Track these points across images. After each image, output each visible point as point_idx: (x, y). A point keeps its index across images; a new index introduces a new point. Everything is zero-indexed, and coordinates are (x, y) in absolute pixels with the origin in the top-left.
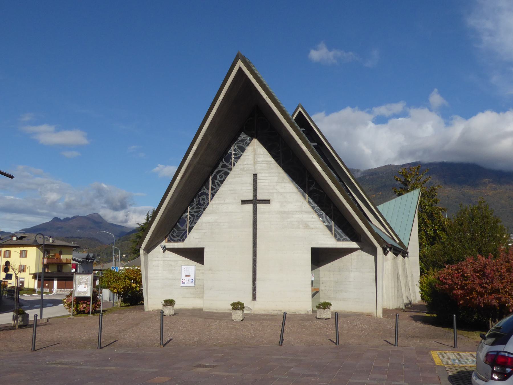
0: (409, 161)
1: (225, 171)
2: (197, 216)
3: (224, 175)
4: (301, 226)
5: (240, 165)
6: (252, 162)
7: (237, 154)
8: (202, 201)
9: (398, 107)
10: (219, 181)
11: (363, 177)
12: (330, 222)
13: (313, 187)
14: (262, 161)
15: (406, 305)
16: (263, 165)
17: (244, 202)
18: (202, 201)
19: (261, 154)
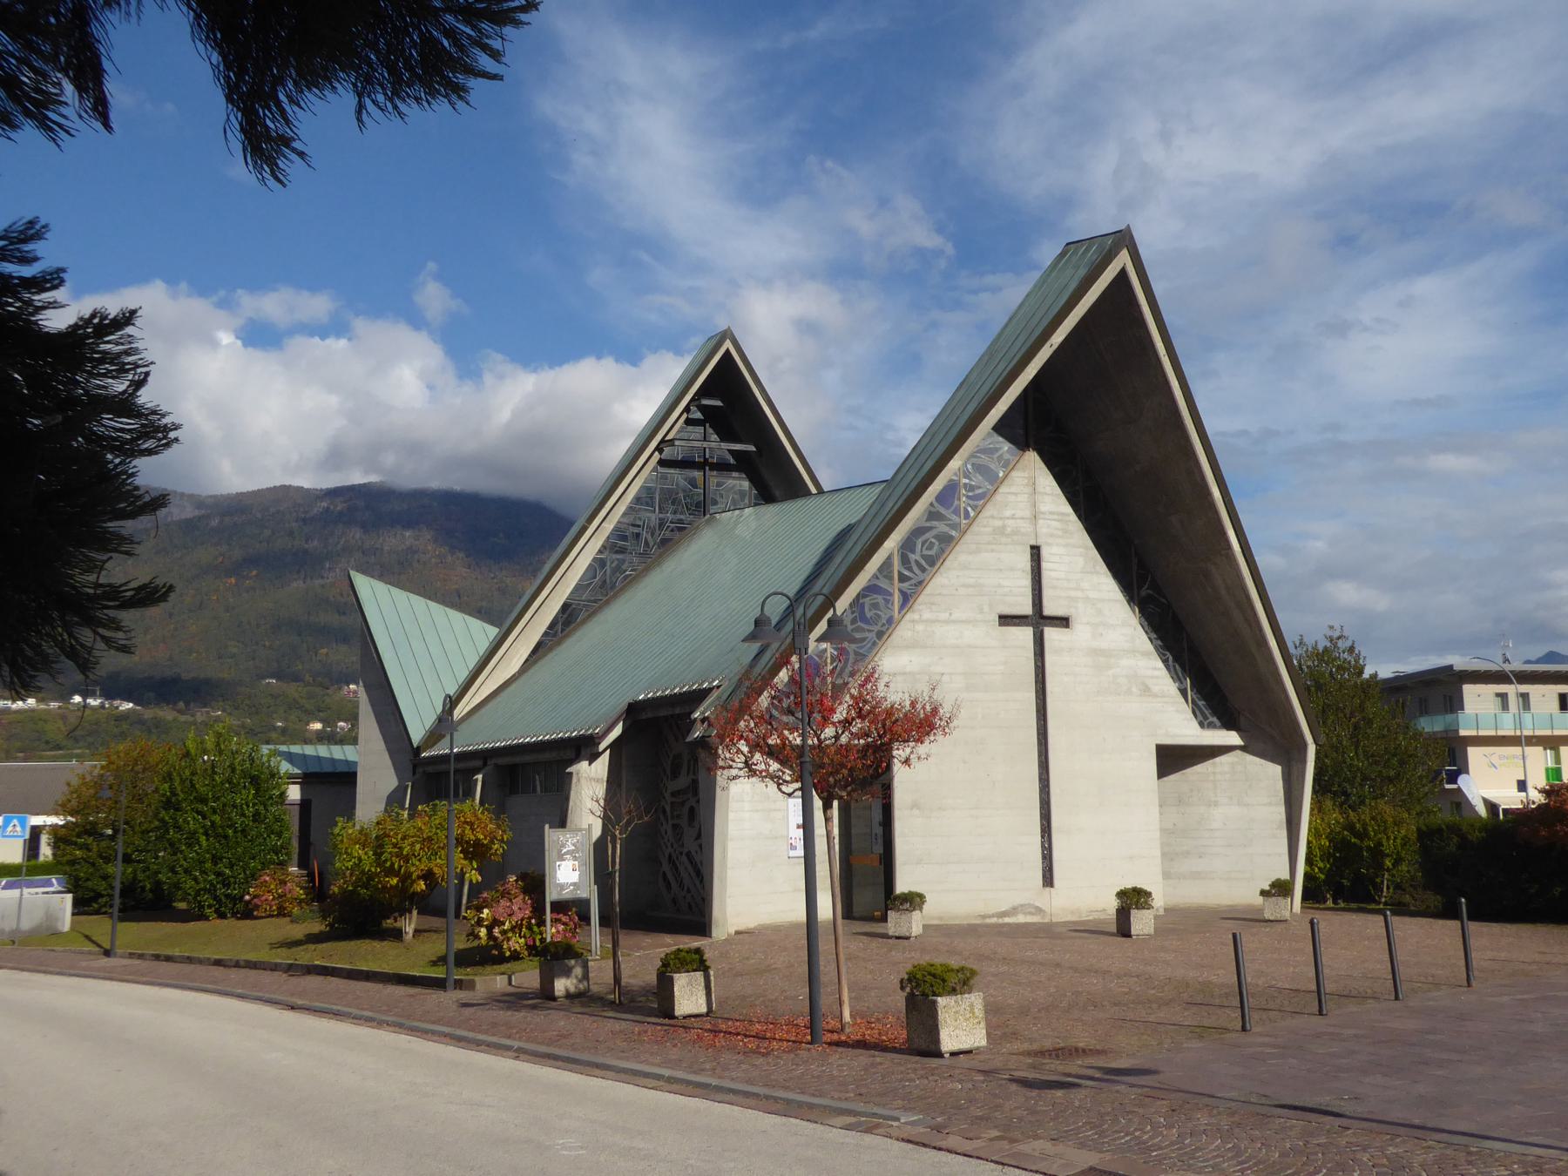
0: (357, 478)
1: (938, 530)
2: (856, 653)
3: (939, 540)
4: (1134, 689)
5: (993, 517)
6: (1027, 513)
7: (974, 486)
8: (870, 610)
9: (318, 305)
10: (923, 556)
11: (200, 518)
12: (1183, 679)
13: (1147, 589)
14: (1051, 513)
15: (1273, 885)
16: (1054, 523)
17: (1006, 620)
18: (870, 610)
19: (1046, 494)
